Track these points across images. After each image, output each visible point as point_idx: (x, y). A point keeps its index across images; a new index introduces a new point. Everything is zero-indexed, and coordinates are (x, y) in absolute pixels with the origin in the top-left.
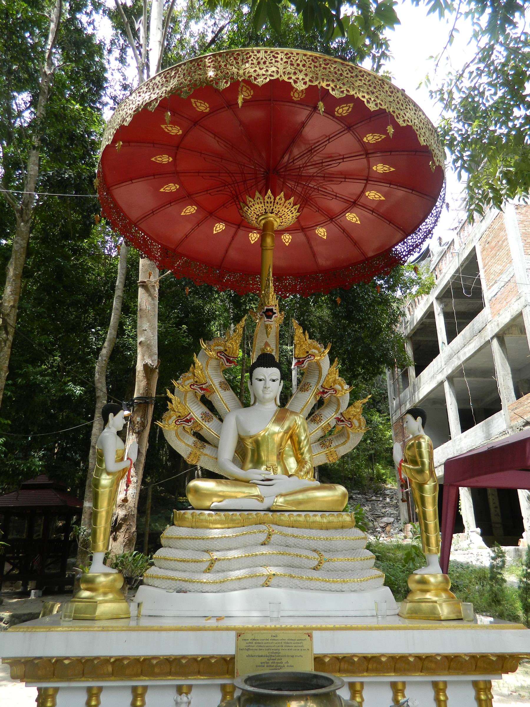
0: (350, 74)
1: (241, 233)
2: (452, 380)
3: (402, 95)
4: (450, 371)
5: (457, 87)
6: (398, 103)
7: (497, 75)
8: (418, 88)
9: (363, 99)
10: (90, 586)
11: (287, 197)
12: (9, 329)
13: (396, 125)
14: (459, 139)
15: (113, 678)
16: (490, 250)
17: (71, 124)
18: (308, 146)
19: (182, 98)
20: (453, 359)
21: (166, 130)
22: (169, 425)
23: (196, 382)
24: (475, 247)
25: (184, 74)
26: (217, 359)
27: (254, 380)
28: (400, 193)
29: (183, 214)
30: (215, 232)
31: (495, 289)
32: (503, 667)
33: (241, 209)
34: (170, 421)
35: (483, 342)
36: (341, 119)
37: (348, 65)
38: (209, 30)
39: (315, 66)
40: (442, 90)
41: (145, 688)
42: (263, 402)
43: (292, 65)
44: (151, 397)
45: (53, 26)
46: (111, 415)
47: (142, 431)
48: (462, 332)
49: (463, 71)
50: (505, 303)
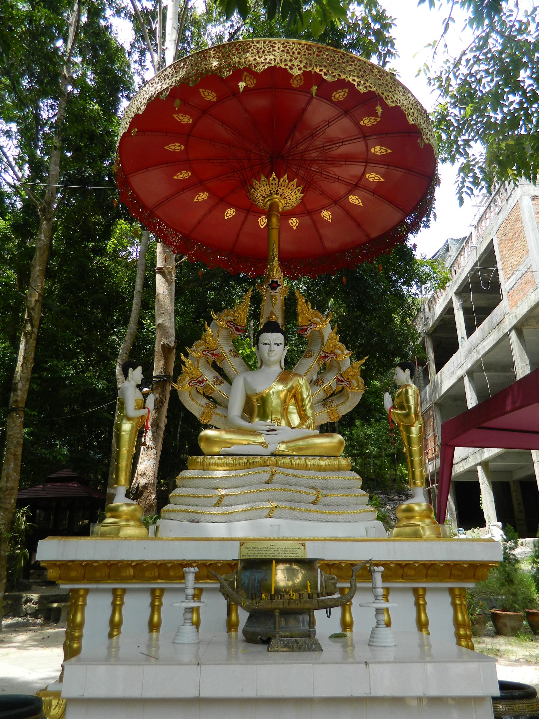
0: (341, 60)
1: (250, 218)
2: (472, 375)
3: (391, 78)
4: (469, 366)
5: (455, 74)
6: (387, 85)
7: (495, 62)
8: (418, 75)
9: (353, 82)
10: (114, 514)
11: (290, 180)
12: (34, 322)
13: (385, 106)
14: (455, 124)
15: (134, 581)
16: (507, 242)
17: (91, 124)
18: (309, 132)
19: (191, 87)
20: (473, 353)
21: (178, 119)
22: (183, 386)
23: (208, 348)
24: (492, 240)
25: (192, 65)
26: (227, 328)
27: (261, 345)
28: (398, 173)
29: (195, 200)
30: (226, 218)
31: (512, 280)
32: (474, 575)
33: (249, 192)
34: (184, 383)
35: (501, 334)
36: (337, 104)
37: (339, 52)
38: (225, 32)
39: (309, 54)
40: (440, 77)
41: (162, 590)
42: (268, 365)
43: (288, 53)
44: (169, 376)
45: (71, 29)
46: (130, 370)
47: (161, 407)
48: (481, 326)
49: (460, 59)
50: (522, 294)
